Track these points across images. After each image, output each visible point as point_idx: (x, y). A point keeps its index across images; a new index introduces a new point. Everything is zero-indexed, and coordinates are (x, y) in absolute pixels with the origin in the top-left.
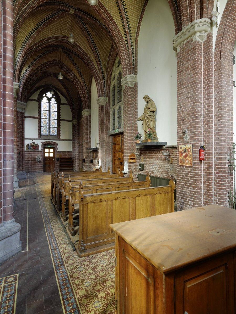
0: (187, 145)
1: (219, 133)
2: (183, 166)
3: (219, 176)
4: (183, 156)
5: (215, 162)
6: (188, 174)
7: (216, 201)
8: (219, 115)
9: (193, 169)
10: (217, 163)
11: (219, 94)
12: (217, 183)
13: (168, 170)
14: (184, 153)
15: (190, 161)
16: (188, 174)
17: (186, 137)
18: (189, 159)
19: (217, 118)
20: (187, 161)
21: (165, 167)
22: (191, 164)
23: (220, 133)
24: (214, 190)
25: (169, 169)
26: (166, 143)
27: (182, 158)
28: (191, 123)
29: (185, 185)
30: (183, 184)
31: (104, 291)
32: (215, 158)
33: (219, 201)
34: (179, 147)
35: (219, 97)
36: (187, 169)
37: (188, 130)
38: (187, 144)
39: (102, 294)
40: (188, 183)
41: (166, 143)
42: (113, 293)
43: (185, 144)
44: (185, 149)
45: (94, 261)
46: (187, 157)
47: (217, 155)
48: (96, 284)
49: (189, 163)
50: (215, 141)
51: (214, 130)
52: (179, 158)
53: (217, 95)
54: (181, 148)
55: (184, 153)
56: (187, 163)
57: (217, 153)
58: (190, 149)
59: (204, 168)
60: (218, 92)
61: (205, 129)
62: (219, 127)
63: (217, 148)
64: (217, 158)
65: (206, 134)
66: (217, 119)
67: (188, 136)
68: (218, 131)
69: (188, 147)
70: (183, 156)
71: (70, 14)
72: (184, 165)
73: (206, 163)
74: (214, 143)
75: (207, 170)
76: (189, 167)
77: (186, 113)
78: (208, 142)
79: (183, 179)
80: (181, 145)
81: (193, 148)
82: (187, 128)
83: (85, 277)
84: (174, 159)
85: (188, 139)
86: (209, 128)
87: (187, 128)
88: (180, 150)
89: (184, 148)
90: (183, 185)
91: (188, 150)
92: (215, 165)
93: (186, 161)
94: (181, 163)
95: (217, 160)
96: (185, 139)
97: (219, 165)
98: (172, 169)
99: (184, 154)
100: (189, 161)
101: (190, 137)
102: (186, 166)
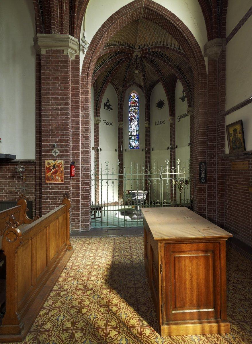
0: (56, 161)
1: (85, 151)
2: (51, 184)
3: (86, 190)
4: (51, 172)
5: (82, 178)
6: (59, 192)
7: (84, 213)
8: (86, 134)
9: (64, 186)
10: (84, 178)
11: (86, 116)
12: (84, 197)
13: (17, 191)
14: (53, 169)
15: (61, 177)
16: (59, 192)
17: (55, 152)
18: (60, 175)
19: (84, 137)
20: (57, 178)
21: (13, 186)
22: (62, 181)
23: (87, 151)
24: (82, 204)
25: (20, 188)
26: (15, 156)
27: (49, 174)
28: (61, 137)
29: (54, 204)
30: (51, 203)
31: (110, 330)
32: (82, 174)
33: (86, 213)
34: (45, 162)
35: (85, 118)
36: (56, 187)
37: (57, 145)
38: (56, 159)
39: (113, 333)
40: (56, 202)
41: (15, 156)
42: (117, 324)
43: (54, 160)
44: (55, 165)
45: (48, 326)
46: (57, 174)
47: (84, 171)
48: (94, 335)
49: (60, 180)
50: (82, 158)
51: (81, 148)
52: (45, 174)
53: (83, 116)
54: (49, 164)
55: (53, 169)
56: (57, 180)
57: (84, 169)
58: (60, 164)
59: (72, 184)
60: (85, 114)
61: (74, 146)
62: (86, 146)
63: (84, 165)
64: (84, 174)
65: (74, 150)
66: (84, 138)
67: (57, 151)
68: (85, 150)
69: (58, 162)
70: (51, 172)
71: (160, 13)
72: (52, 182)
73: (74, 179)
74: (81, 160)
75: (76, 186)
76: (60, 184)
77: (55, 126)
78: (77, 159)
79: (51, 198)
80: (47, 159)
81: (65, 164)
82: (56, 142)
83: (152, 305)
84: (28, 177)
85: (57, 154)
86: (78, 145)
87: (56, 142)
88: (46, 165)
89: (53, 164)
90: (51, 204)
91: (58, 166)
92: (82, 181)
93: (55, 178)
94: (47, 180)
95: (84, 176)
96: (54, 154)
97: (86, 180)
98: (26, 189)
99: (53, 170)
100: (60, 177)
101: (61, 152)
102: (54, 184)
